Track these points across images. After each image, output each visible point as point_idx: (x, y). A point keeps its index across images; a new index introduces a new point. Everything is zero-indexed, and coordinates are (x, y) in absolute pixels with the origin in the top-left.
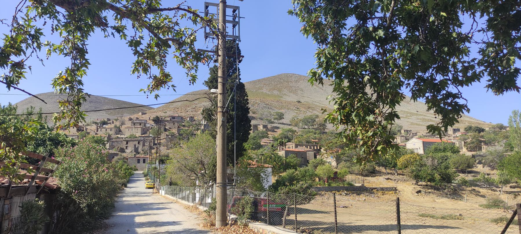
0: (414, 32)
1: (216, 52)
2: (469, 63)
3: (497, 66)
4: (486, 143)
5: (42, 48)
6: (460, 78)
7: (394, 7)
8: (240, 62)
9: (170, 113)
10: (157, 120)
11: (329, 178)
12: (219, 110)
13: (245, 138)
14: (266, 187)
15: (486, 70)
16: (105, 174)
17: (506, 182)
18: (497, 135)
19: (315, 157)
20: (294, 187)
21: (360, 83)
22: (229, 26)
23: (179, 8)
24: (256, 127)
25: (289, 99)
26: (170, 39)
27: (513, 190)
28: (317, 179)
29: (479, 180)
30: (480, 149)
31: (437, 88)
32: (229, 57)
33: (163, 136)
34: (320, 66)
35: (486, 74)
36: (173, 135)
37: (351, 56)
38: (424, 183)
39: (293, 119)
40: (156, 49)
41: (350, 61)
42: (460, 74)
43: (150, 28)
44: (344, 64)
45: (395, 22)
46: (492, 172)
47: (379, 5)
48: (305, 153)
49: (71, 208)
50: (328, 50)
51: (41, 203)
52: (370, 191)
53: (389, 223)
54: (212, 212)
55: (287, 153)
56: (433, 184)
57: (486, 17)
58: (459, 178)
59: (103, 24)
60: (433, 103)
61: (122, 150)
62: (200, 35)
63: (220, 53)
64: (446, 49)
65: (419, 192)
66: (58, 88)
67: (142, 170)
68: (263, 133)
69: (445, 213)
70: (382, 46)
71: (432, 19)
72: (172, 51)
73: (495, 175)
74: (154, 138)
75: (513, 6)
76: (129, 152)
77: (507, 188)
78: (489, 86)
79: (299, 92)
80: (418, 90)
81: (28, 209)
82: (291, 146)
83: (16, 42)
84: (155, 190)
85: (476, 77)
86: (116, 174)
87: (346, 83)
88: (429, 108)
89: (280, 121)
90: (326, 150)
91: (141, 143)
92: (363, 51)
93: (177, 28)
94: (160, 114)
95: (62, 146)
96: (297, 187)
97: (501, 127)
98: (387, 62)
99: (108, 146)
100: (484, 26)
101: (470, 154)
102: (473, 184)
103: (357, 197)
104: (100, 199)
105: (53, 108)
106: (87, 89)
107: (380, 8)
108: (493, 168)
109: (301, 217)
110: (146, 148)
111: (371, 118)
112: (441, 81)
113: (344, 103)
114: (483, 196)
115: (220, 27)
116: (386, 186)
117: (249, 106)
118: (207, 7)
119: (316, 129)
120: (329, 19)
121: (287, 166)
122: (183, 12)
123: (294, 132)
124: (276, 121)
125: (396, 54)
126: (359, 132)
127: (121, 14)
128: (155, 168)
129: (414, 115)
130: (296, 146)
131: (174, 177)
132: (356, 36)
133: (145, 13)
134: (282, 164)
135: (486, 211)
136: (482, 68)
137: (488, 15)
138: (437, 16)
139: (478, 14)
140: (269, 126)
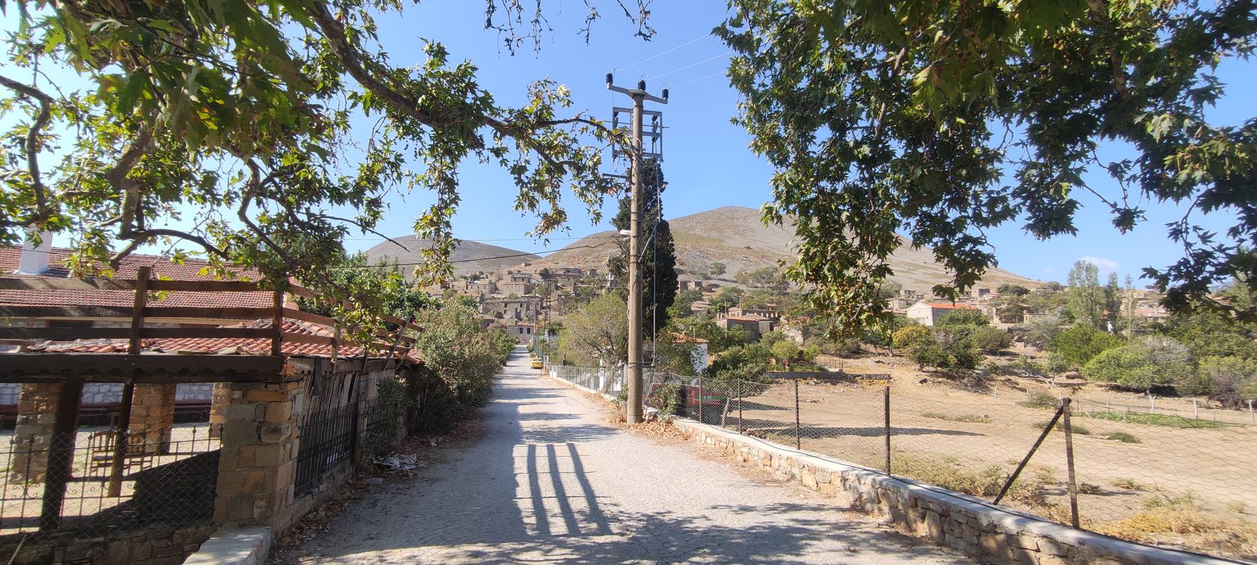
0: (916, 147)
1: (629, 178)
2: (998, 193)
3: (1040, 197)
4: (1030, 311)
5: (403, 179)
6: (984, 215)
7: (885, 112)
8: (662, 190)
9: (563, 264)
10: (545, 274)
11: (791, 359)
12: (632, 259)
13: (669, 300)
14: (699, 370)
15: (1024, 204)
16: (479, 346)
17: (1060, 369)
18: (1048, 298)
19: (772, 329)
20: (737, 372)
21: (835, 222)
22: (647, 140)
23: (577, 119)
24: (685, 284)
25: (733, 244)
26: (565, 162)
27: (1071, 381)
28: (774, 361)
29: (1017, 366)
30: (1021, 319)
31: (948, 229)
32: (647, 184)
33: (554, 295)
34: (778, 197)
35: (1024, 209)
36: (567, 295)
37: (823, 184)
38: (932, 369)
39: (739, 274)
40: (546, 176)
41: (821, 191)
42: (984, 209)
43: (539, 148)
44: (813, 195)
45: (886, 133)
46: (1038, 355)
47: (863, 110)
48: (756, 323)
49: (438, 390)
50: (787, 173)
51: (402, 381)
52: (852, 379)
53: (875, 425)
54: (622, 403)
55: (730, 323)
56: (945, 370)
57: (1025, 125)
58: (986, 362)
59: (478, 144)
60: (943, 252)
61: (500, 316)
62: (606, 155)
63: (634, 180)
64: (964, 172)
65: (924, 381)
66: (421, 232)
67: (526, 342)
68: (695, 292)
69: (961, 412)
70: (868, 169)
71: (943, 128)
72: (569, 176)
73: (1044, 359)
74: (542, 300)
75: (1066, 107)
76: (508, 318)
77: (1062, 378)
78: (1029, 227)
79: (749, 233)
80: (921, 233)
81: (386, 388)
82: (736, 313)
83: (372, 173)
84: (543, 371)
85: (1009, 213)
86: (493, 346)
87: (815, 223)
88: (939, 259)
89: (721, 277)
90: (787, 319)
91: (525, 306)
92: (839, 176)
93: (575, 146)
94: (550, 266)
95: (425, 308)
96: (743, 370)
97: (1056, 287)
98: (874, 192)
99: (481, 308)
100: (1024, 138)
101: (1005, 327)
102: (1006, 371)
103: (832, 388)
104: (473, 379)
105: (417, 258)
106: (456, 233)
107: (864, 114)
108: (1041, 349)
109: (748, 415)
110: (532, 312)
111: (850, 272)
112: (956, 220)
113: (813, 250)
114: (1023, 390)
115: (635, 144)
116: (875, 372)
117: (676, 254)
118: (616, 114)
119: (773, 288)
120: (791, 130)
121: (729, 342)
122: (585, 125)
123: (740, 292)
124: (714, 276)
125: (887, 181)
126: (833, 293)
127: (502, 130)
128: (544, 341)
129: (914, 269)
130: (744, 313)
131: (569, 353)
132: (830, 154)
133: (533, 128)
134: (723, 338)
135: (1027, 411)
136: (1019, 200)
137: (1030, 119)
138: (952, 125)
139: (1015, 119)
140: (704, 284)
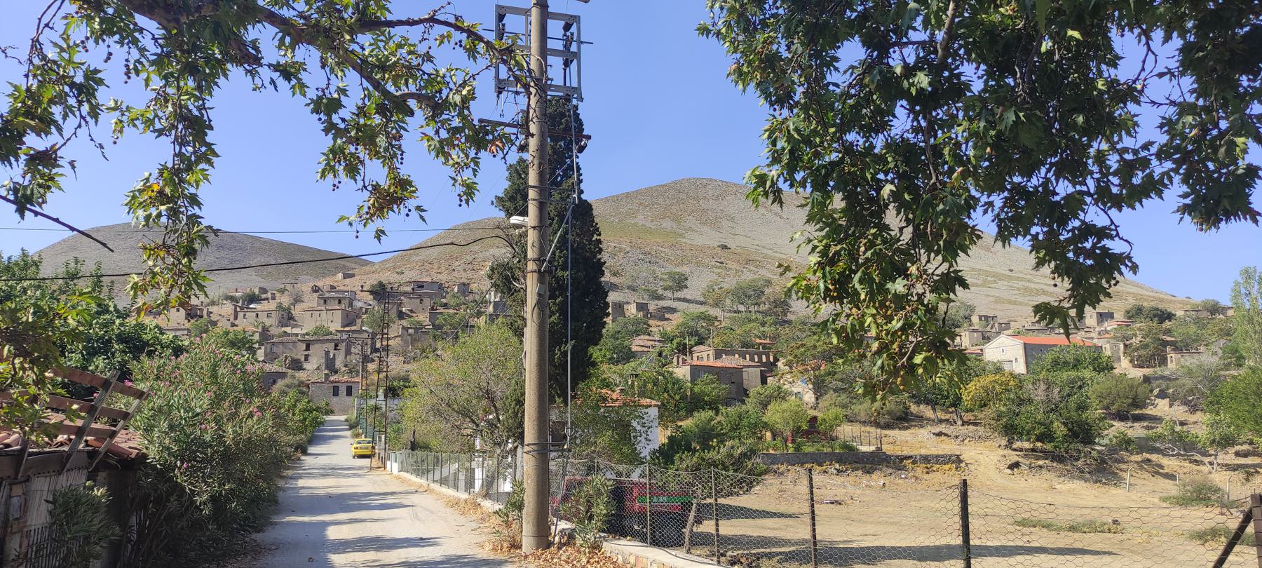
0: (1002, 77)
1: (524, 126)
2: (1135, 152)
3: (1203, 161)
4: (1177, 348)
5: (103, 117)
6: (1115, 190)
7: (954, 16)
8: (581, 149)
9: (412, 275)
10: (381, 292)
11: (797, 431)
12: (531, 266)
13: (594, 335)
14: (645, 453)
15: (1176, 171)
16: (253, 422)
17: (1226, 442)
18: (1204, 327)
19: (764, 382)
20: (711, 455)
21: (871, 200)
22: (556, 63)
23: (433, 20)
24: (620, 307)
25: (699, 240)
26: (411, 95)
27: (1242, 461)
28: (768, 435)
29: (1160, 437)
30: (1163, 361)
31: (1059, 213)
32: (555, 139)
33: (395, 330)
34: (776, 160)
35: (1177, 179)
36: (419, 328)
37: (851, 137)
38: (1027, 445)
39: (710, 289)
40: (377, 120)
41: (848, 149)
42: (1115, 180)
43: (364, 68)
44: (834, 156)
45: (956, 53)
46: (1192, 418)
47: (917, 12)
48: (738, 371)
49: (173, 505)
50: (794, 120)
51: (99, 492)
52: (897, 463)
53: (943, 542)
54: (513, 514)
55: (696, 371)
56: (1048, 447)
57: (1177, 42)
58: (1111, 432)
59: (250, 58)
60: (1048, 251)
61: (297, 365)
62: (485, 85)
63: (533, 128)
64: (1080, 119)
65: (1014, 466)
66: (141, 213)
67: (344, 412)
68: (636, 322)
69: (1078, 516)
70: (926, 112)
71: (1046, 45)
72: (417, 124)
73: (1200, 425)
74: (373, 336)
75: (1242, 14)
76: (313, 369)
77: (1229, 457)
78: (1185, 209)
79: (725, 223)
80: (1012, 219)
81: (67, 507)
82: (705, 355)
83: (38, 103)
84: (375, 462)
85: (1153, 187)
86: (280, 422)
87: (838, 202)
88: (1040, 263)
89: (679, 295)
90: (789, 364)
91: (342, 347)
92: (880, 123)
93: (428, 67)
94: (388, 277)
95: (150, 354)
96: (719, 453)
97: (1215, 309)
98: (937, 151)
99: (260, 354)
100: (1173, 64)
101: (1137, 373)
102: (1145, 446)
103: (865, 479)
104: (242, 482)
105: (129, 262)
106: (211, 215)
107: (920, 19)
108: (1194, 409)
109: (729, 528)
110: (355, 359)
111: (899, 286)
112: (1068, 197)
113: (833, 250)
114: (1170, 477)
115: (533, 66)
116: (934, 452)
117: (604, 256)
118: (501, 18)
119: (765, 314)
120: (798, 47)
121: (694, 403)
122: (444, 30)
123: (711, 320)
124: (668, 294)
125: (959, 132)
126: (869, 320)
127: (294, 33)
128: (376, 408)
129: (1002, 280)
130: (718, 355)
131: (421, 429)
132: (862, 86)
133: (352, 32)
134: (684, 398)
135: (1178, 512)
136: (1169, 165)
137: (1182, 35)
138: (1059, 38)
139: (1158, 35)
140: (652, 306)
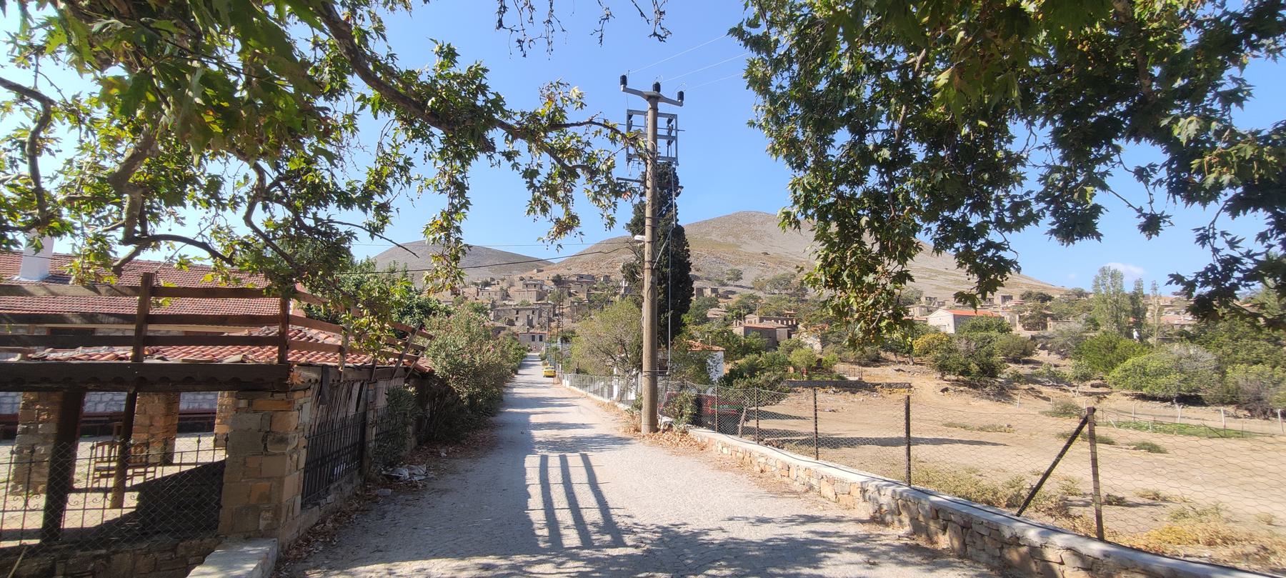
0: (937, 151)
1: (644, 182)
2: (1021, 197)
3: (1064, 202)
4: (1054, 318)
5: (413, 183)
6: (1007, 220)
7: (906, 114)
8: (677, 195)
9: (576, 270)
10: (558, 281)
11: (809, 368)
12: (647, 265)
13: (684, 307)
14: (715, 379)
15: (1047, 208)
16: (490, 354)
17: (1085, 378)
18: (1073, 305)
19: (789, 337)
20: (754, 380)
21: (855, 227)
22: (662, 143)
23: (591, 122)
24: (700, 291)
25: (750, 249)
26: (578, 166)
27: (1095, 390)
28: (791, 369)
29: (1040, 374)
30: (1045, 327)
31: (970, 235)
32: (662, 189)
33: (567, 302)
34: (796, 202)
35: (1048, 213)
36: (580, 302)
37: (842, 188)
38: (953, 377)
39: (756, 280)
40: (559, 181)
41: (840, 195)
42: (1007, 214)
43: (552, 151)
44: (832, 200)
45: (907, 137)
46: (1062, 363)
47: (883, 112)
48: (774, 330)
49: (449, 399)
50: (805, 177)
51: (411, 390)
52: (871, 388)
53: (895, 435)
54: (636, 412)
55: (747, 330)
56: (967, 379)
57: (1049, 128)
58: (1008, 370)
59: (489, 147)
60: (965, 258)
61: (511, 323)
62: (620, 158)
63: (649, 184)
64: (986, 176)
65: (946, 390)
66: (431, 237)
67: (538, 350)
68: (711, 299)
69: (983, 421)
70: (888, 172)
71: (965, 131)
72: (582, 180)
73: (1068, 367)
74: (554, 307)
75: (1091, 110)
76: (520, 326)
77: (1087, 387)
78: (1053, 232)
79: (766, 238)
80: (942, 239)
81: (395, 397)
82: (753, 320)
83: (381, 177)
84: (555, 380)
85: (1032, 218)
86: (504, 354)
87: (834, 228)
88: (960, 265)
89: (738, 283)
90: (806, 326)
91: (537, 313)
92: (859, 180)
93: (588, 150)
94: (563, 272)
95: (435, 315)
96: (760, 379)
97: (1081, 294)
98: (894, 196)
99: (492, 315)
100: (1048, 141)
101: (1028, 334)
102: (1030, 379)
103: (851, 397)
104: (484, 388)
105: (427, 264)
106: (467, 238)
107: (884, 117)
108: (1065, 357)
109: (765, 425)
110: (544, 320)
111: (870, 279)
112: (978, 226)
113: (831, 256)
114: (1047, 399)
115: (649, 147)
116: (895, 381)
117: (691, 259)
118: (630, 117)
119: (791, 295)
120: (809, 133)
121: (746, 350)
122: (598, 128)
123: (757, 299)
124: (731, 282)
125: (908, 186)
126: (852, 300)
127: (513, 133)
128: (556, 349)
129: (935, 275)
130: (761, 320)
131: (583, 362)
132: (849, 157)
133: (545, 131)
134: (740, 346)
135: (1051, 421)
136: (1042, 205)
137: (1053, 122)
138: (974, 128)
139: (1039, 122)
140: (721, 291)
